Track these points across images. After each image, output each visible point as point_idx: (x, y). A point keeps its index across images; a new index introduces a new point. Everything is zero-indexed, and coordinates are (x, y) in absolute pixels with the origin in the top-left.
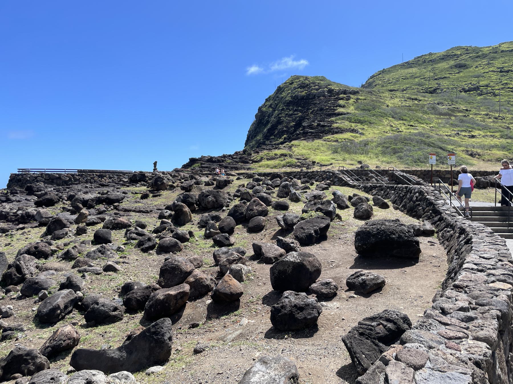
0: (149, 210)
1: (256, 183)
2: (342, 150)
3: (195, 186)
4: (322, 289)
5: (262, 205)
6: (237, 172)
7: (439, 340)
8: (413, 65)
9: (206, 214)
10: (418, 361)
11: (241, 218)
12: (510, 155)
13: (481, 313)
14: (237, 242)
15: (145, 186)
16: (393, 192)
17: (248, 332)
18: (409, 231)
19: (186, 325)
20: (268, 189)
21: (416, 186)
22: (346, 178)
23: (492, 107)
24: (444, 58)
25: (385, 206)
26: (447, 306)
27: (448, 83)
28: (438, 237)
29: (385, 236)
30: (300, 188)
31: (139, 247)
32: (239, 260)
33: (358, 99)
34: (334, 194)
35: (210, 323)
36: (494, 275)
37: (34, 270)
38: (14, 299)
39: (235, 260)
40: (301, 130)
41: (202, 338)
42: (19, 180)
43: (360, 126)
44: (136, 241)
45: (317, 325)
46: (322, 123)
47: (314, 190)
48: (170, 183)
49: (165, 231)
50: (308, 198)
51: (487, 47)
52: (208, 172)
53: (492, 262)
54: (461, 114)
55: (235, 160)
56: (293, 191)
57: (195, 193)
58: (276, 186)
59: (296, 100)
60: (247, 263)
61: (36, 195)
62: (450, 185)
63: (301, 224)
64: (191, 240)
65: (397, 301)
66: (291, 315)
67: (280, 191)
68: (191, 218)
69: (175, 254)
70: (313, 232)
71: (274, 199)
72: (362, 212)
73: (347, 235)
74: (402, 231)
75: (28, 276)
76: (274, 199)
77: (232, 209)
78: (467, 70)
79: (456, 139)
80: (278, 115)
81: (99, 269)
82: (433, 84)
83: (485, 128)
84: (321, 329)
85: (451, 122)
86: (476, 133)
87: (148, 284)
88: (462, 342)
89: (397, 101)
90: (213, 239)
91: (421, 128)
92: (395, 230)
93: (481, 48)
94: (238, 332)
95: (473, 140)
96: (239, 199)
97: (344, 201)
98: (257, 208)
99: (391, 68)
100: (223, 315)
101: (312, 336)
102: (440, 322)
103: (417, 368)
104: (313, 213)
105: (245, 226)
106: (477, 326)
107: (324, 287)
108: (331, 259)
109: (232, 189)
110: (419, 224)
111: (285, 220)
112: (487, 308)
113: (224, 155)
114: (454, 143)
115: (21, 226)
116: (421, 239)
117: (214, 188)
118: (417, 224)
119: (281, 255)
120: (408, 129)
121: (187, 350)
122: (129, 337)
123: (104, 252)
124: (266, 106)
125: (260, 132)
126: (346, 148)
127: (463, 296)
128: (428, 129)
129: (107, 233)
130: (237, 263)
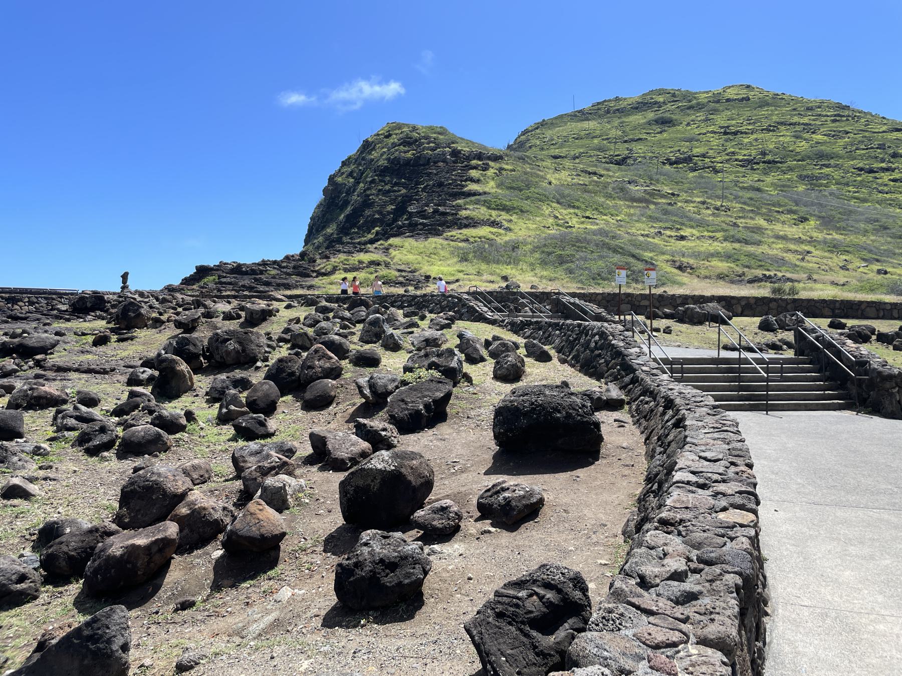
0: (107, 367)
1: (322, 316)
2: (475, 257)
3: (204, 320)
4: (434, 519)
5: (331, 358)
6: (288, 293)
7: (637, 651)
8: (590, 117)
9: (223, 376)
11: (289, 381)
12: (738, 269)
13: (708, 581)
14: (282, 429)
15: (103, 319)
16: (557, 332)
17: (290, 615)
18: (584, 406)
19: (168, 605)
20: (344, 327)
21: (595, 323)
22: (481, 308)
23: (711, 190)
24: (640, 106)
25: (544, 357)
26: (650, 569)
27: (644, 149)
28: (630, 411)
29: (544, 415)
30: (402, 324)
31: (80, 445)
32: (283, 468)
33: (501, 169)
34: (460, 336)
35: (219, 598)
36: (724, 495)
39: (273, 468)
40: (406, 220)
41: (200, 631)
43: (504, 216)
44: (75, 434)
45: (422, 594)
46: (441, 209)
47: (425, 329)
48: (154, 315)
49: (136, 412)
50: (416, 343)
51: (704, 92)
52: (233, 293)
53: (719, 467)
54: (664, 201)
55: (285, 270)
56: (389, 330)
57: (202, 335)
58: (359, 322)
59: (396, 165)
62: (647, 318)
63: (401, 393)
64: (189, 427)
65: (564, 536)
66: (373, 578)
67: (365, 331)
68: (193, 384)
69: (156, 456)
70: (421, 407)
71: (355, 346)
72: (507, 369)
73: (482, 410)
74: (572, 406)
76: (355, 346)
77: (273, 365)
78: (674, 129)
80: (365, 191)
82: (622, 150)
83: (700, 224)
84: (429, 601)
85: (649, 213)
86: (686, 232)
87: (95, 523)
88: (678, 652)
89: (565, 176)
90: (233, 425)
91: (603, 222)
92: (561, 405)
93: (696, 93)
94: (270, 618)
95: (683, 243)
96: (289, 346)
97: (476, 350)
98: (321, 363)
99: (556, 118)
100: (245, 580)
101: (411, 617)
102: (638, 607)
104: (423, 373)
105: (297, 398)
106: (703, 611)
107: (436, 516)
108: (453, 457)
109: (275, 327)
110: (599, 390)
111: (372, 386)
112: (717, 569)
113: (263, 261)
114: (653, 248)
117: (242, 325)
118: (597, 389)
119: (364, 455)
120: (583, 223)
121: (162, 664)
123: (5, 457)
124: (343, 173)
126: (482, 253)
127: (675, 543)
128: (614, 224)
129: (14, 418)
130: (277, 474)
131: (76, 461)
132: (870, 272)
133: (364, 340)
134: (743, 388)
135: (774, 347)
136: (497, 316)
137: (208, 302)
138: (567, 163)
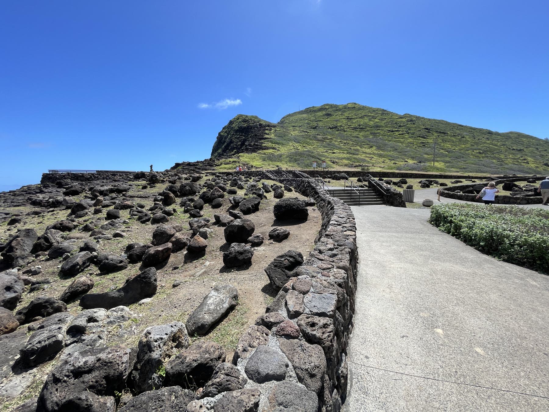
0: (147, 196)
9: (185, 198)
10: (305, 288)
11: (208, 199)
24: (321, 109)
25: (290, 190)
26: (322, 248)
32: (205, 225)
33: (276, 130)
34: (263, 184)
37: (59, 239)
38: (43, 261)
42: (50, 178)
43: (277, 146)
44: (137, 217)
47: (251, 182)
57: (178, 185)
60: (211, 227)
61: (64, 188)
64: (175, 214)
66: (235, 258)
67: (232, 183)
71: (228, 187)
74: (299, 204)
75: (55, 244)
76: (228, 187)
79: (326, 154)
81: (110, 236)
82: (315, 124)
83: (340, 148)
84: (253, 264)
91: (309, 148)
94: (203, 271)
102: (318, 259)
103: (305, 293)
104: (251, 196)
109: (202, 182)
111: (234, 200)
112: (343, 247)
115: (51, 209)
116: (308, 208)
119: (232, 221)
121: (168, 285)
122: (127, 281)
125: (220, 148)
127: (330, 241)
129: (116, 212)
131: (138, 225)
132: (391, 163)
133: (231, 186)
134: (352, 198)
135: (362, 187)
136: (275, 178)
137: (179, 174)
138: (297, 128)
